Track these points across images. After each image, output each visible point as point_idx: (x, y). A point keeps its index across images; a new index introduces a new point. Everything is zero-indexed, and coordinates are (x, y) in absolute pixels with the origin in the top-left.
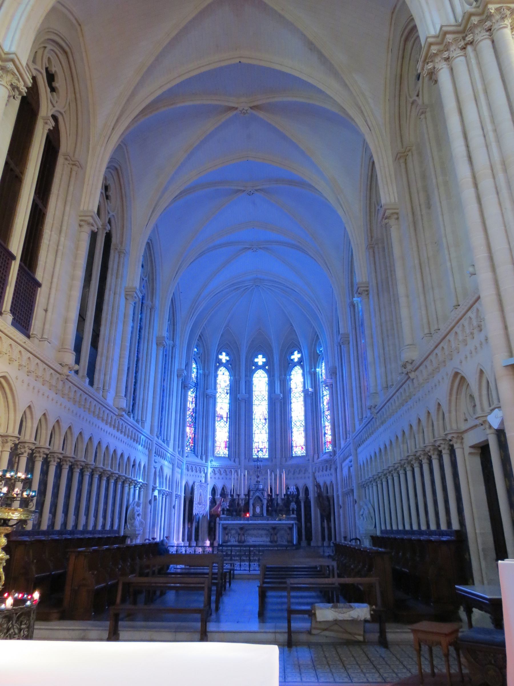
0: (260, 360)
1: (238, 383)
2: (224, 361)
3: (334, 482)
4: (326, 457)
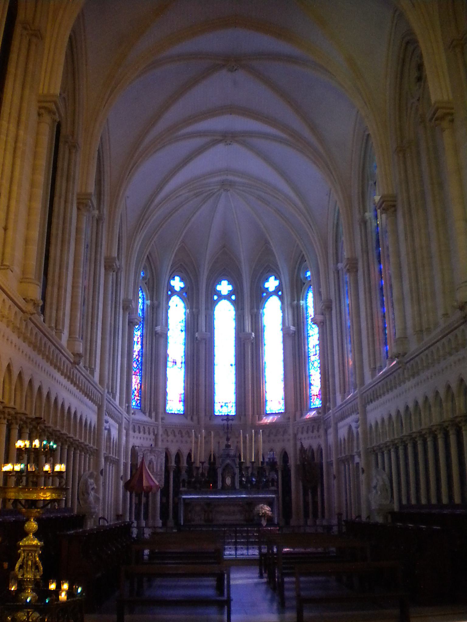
0: (224, 287)
1: (196, 317)
2: (177, 289)
3: (323, 446)
4: (312, 414)
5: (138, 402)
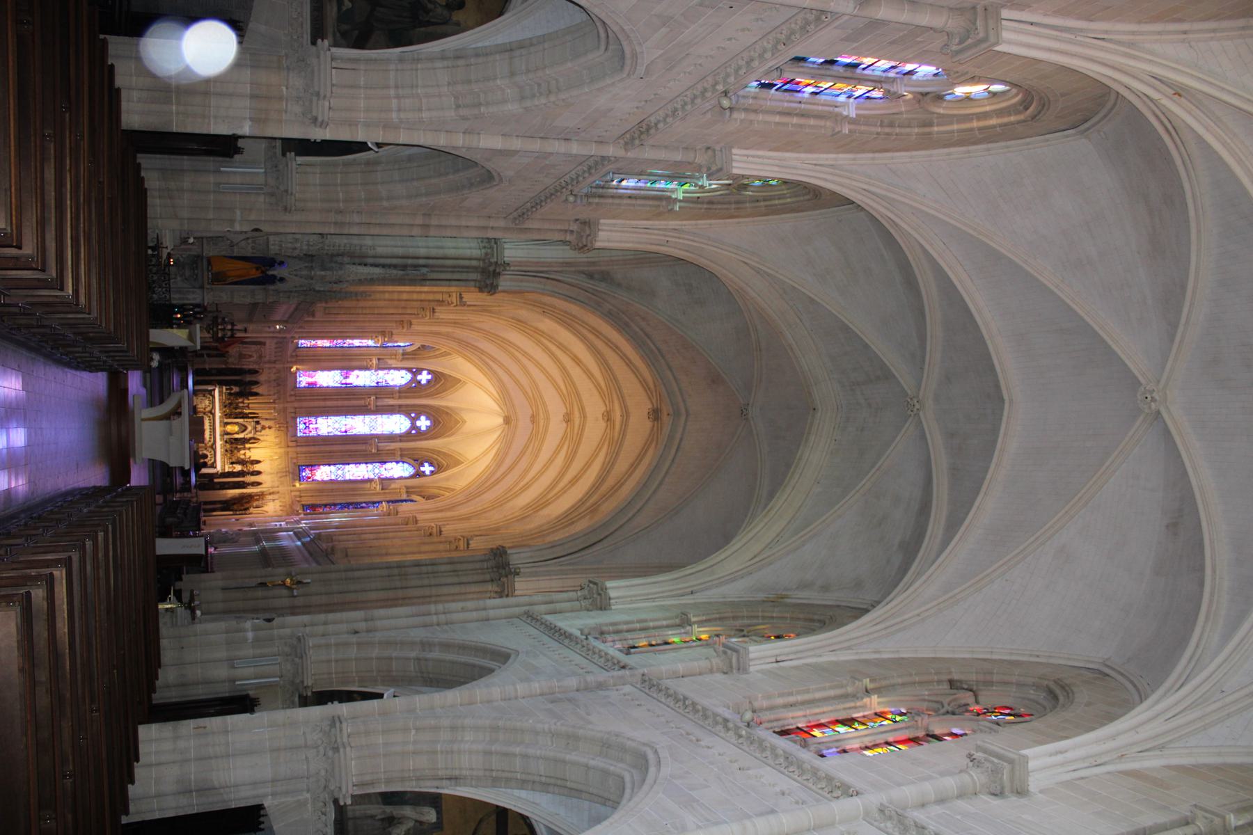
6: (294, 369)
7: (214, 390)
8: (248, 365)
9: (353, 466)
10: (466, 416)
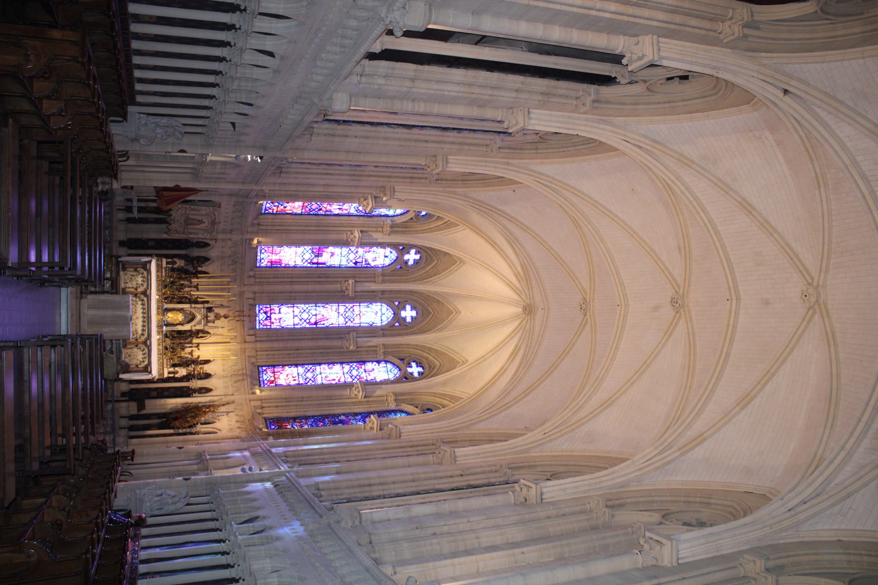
5: (270, 211)
6: (255, 242)
7: (150, 262)
8: (197, 234)
9: (326, 366)
10: (460, 305)
